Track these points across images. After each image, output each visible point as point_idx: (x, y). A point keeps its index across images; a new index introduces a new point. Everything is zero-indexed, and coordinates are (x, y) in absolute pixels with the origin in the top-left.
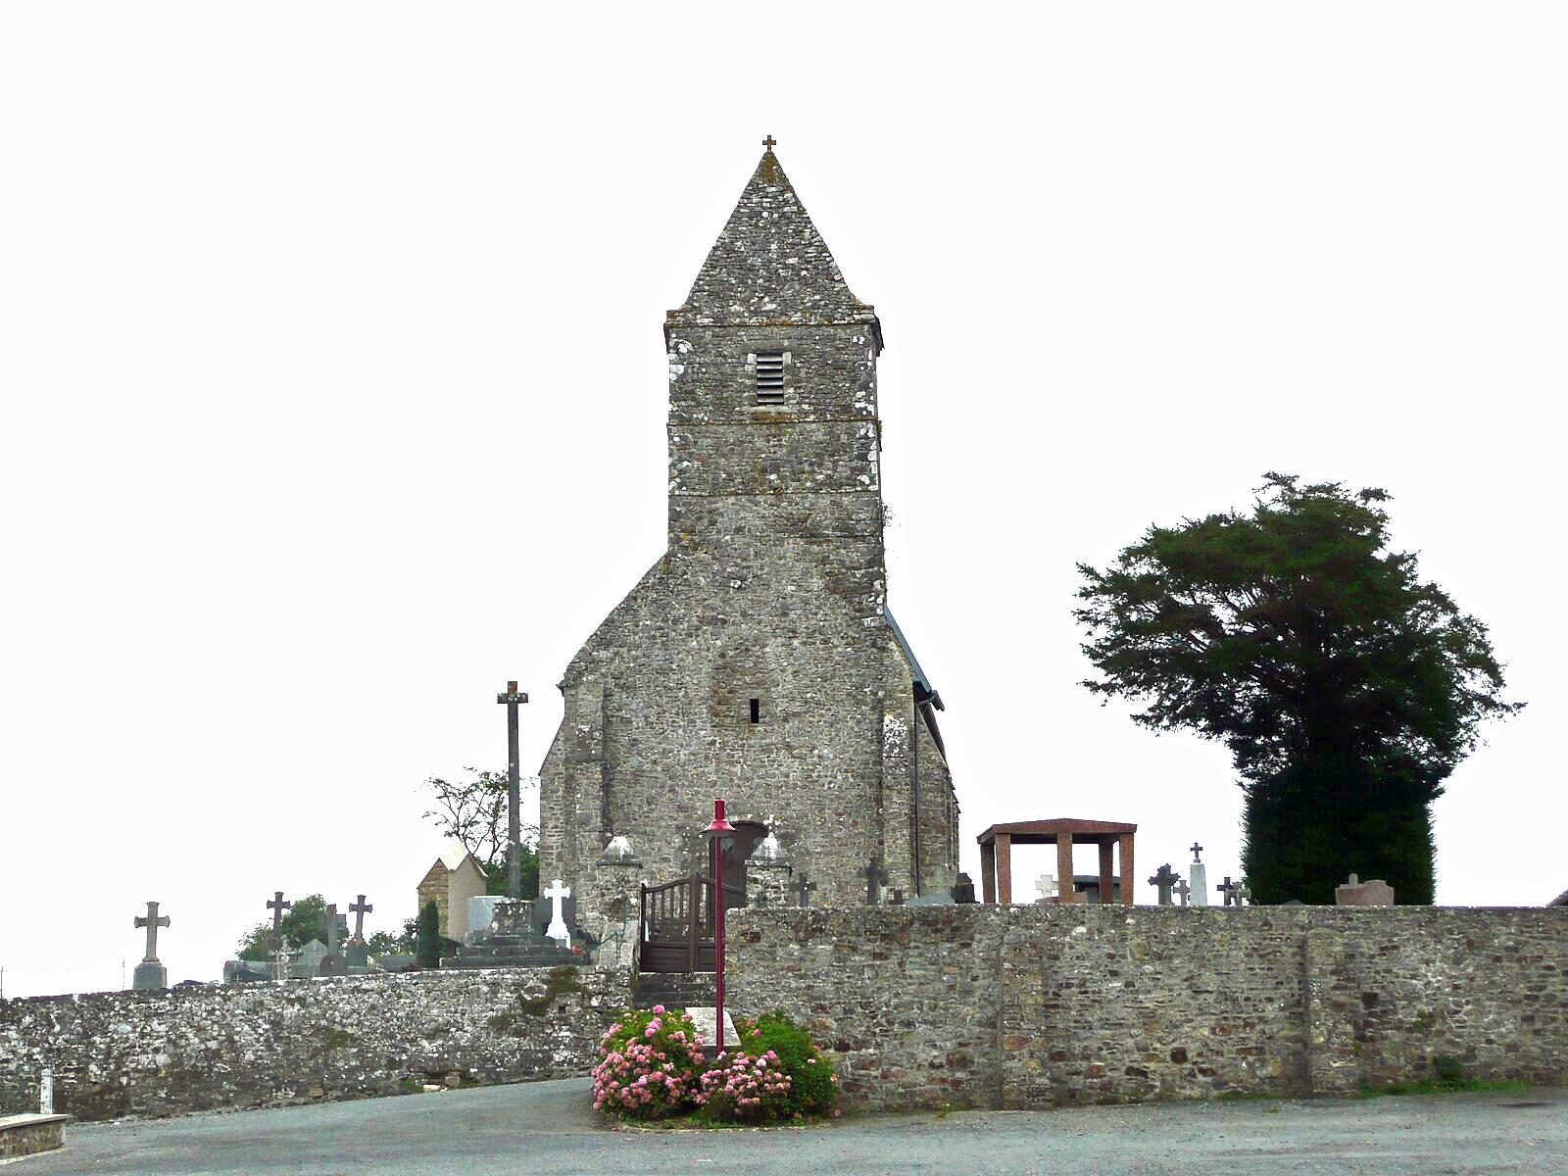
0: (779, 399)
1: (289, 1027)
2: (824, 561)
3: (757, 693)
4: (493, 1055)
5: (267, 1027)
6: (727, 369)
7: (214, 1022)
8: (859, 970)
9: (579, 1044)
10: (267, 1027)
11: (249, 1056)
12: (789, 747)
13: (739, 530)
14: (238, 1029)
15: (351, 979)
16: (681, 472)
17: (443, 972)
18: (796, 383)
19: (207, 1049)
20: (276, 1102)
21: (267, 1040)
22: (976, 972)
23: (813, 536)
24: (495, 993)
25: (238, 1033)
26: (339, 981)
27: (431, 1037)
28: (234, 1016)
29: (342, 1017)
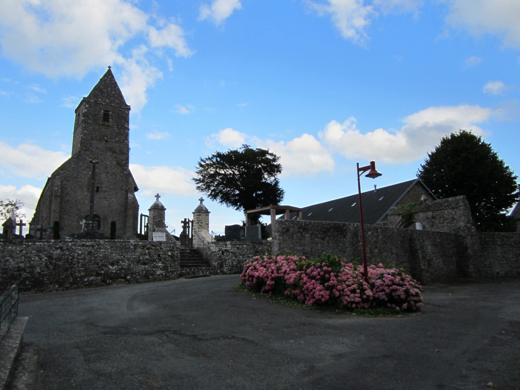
0: (108, 121)
1: (56, 259)
2: (116, 158)
3: (99, 185)
4: (135, 272)
5: (46, 258)
6: (97, 112)
7: (22, 256)
8: (317, 244)
9: (165, 268)
10: (46, 258)
11: (38, 270)
12: (105, 198)
13: (97, 148)
14: (33, 259)
15: (81, 241)
16: (84, 133)
17: (117, 240)
18: (112, 119)
19: (19, 267)
20: (50, 289)
21: (46, 264)
22: (347, 245)
23: (114, 152)
24: (135, 249)
25: (33, 261)
26: (77, 241)
27: (112, 264)
28: (31, 253)
29: (78, 256)
